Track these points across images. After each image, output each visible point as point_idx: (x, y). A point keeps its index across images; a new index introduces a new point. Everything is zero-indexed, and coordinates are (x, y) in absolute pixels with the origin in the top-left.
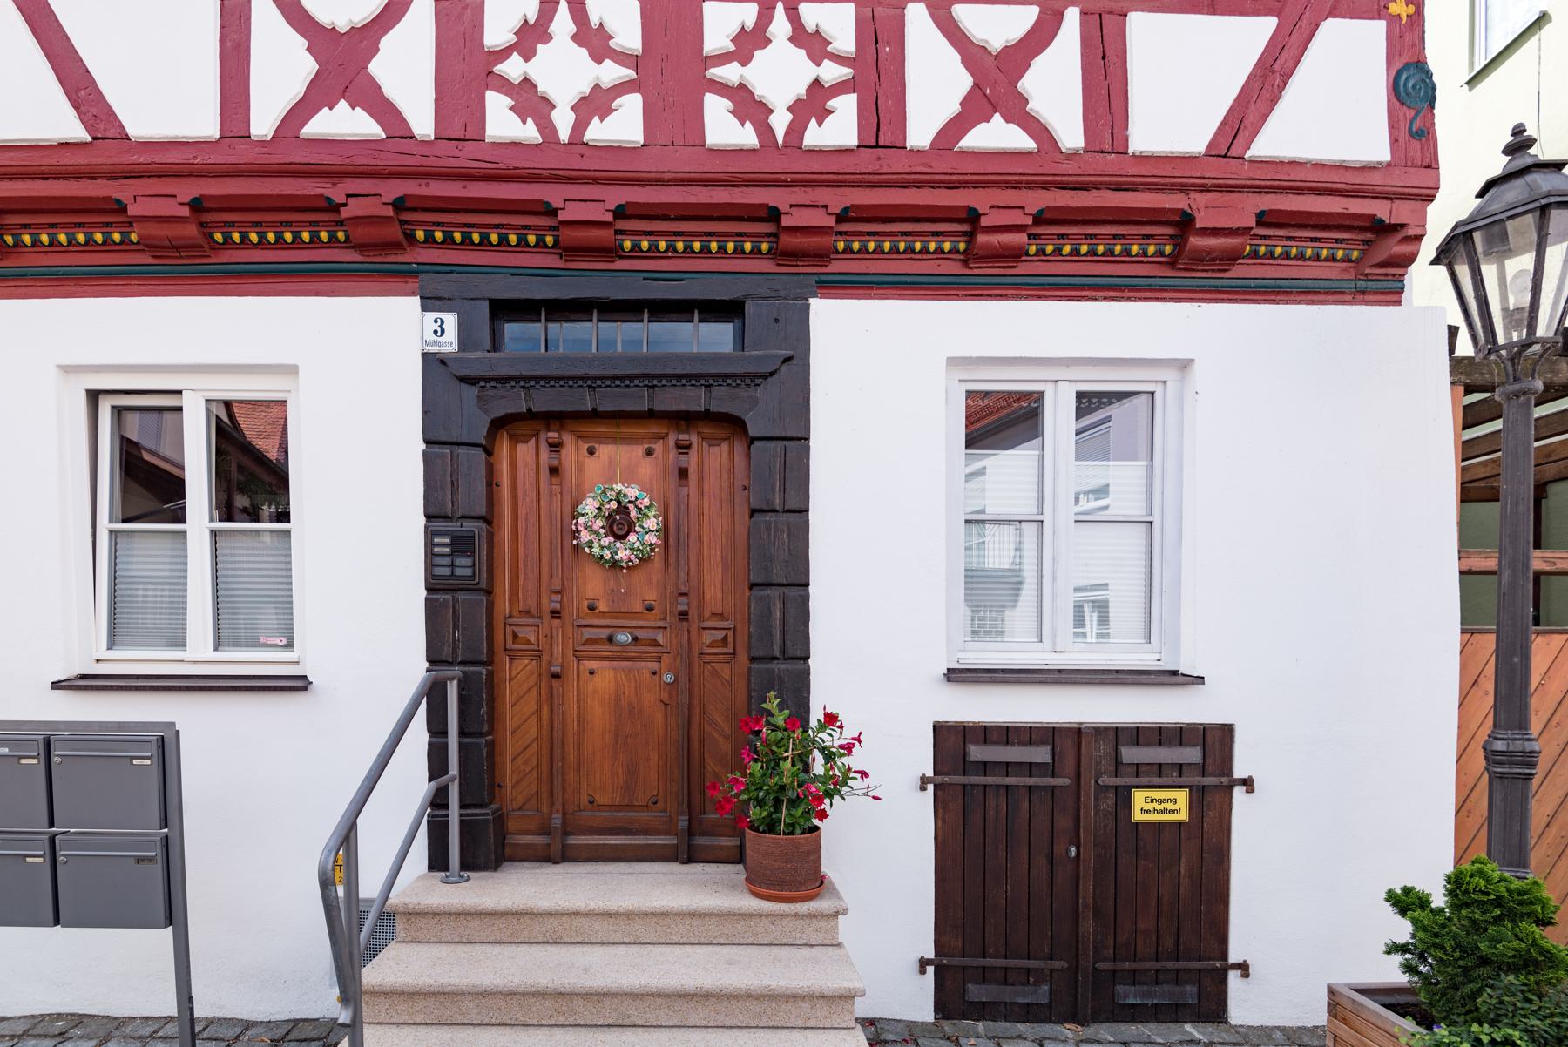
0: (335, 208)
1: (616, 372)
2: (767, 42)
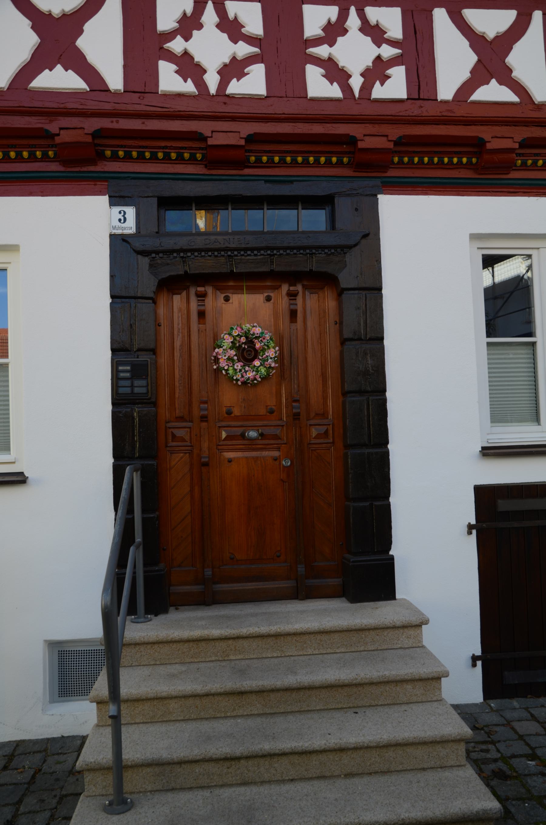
0: (53, 136)
1: (248, 246)
2: (345, 31)
